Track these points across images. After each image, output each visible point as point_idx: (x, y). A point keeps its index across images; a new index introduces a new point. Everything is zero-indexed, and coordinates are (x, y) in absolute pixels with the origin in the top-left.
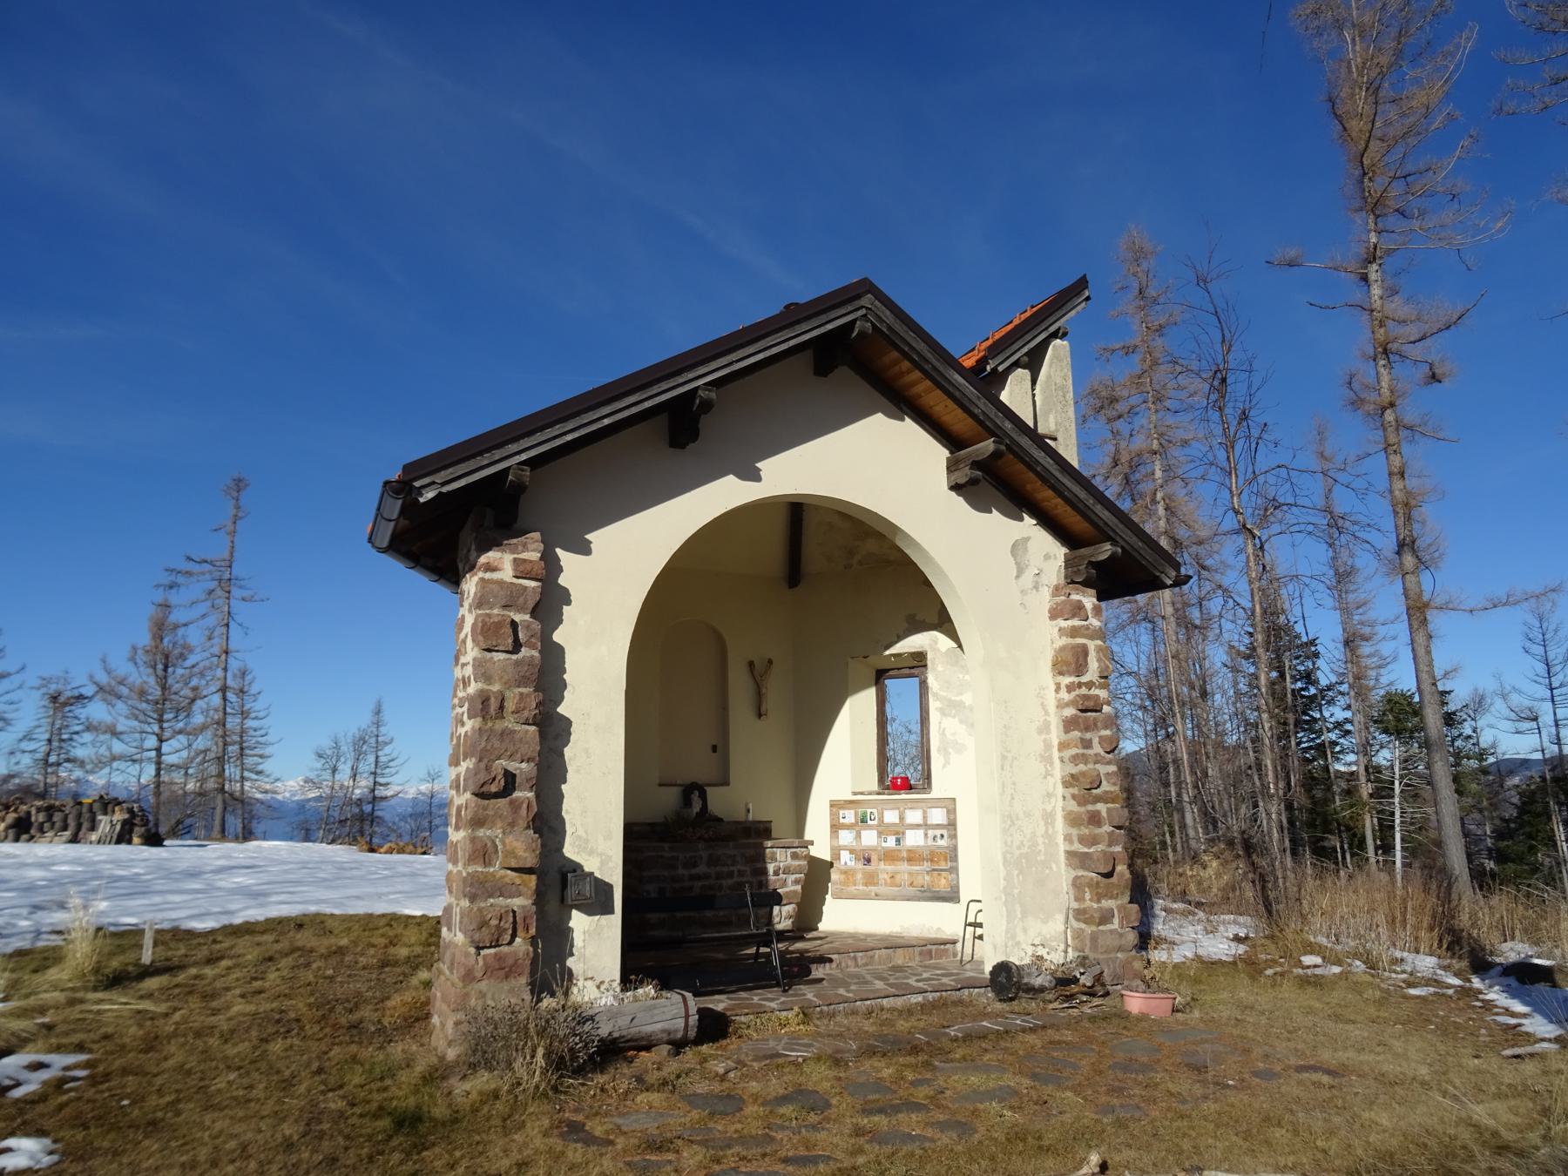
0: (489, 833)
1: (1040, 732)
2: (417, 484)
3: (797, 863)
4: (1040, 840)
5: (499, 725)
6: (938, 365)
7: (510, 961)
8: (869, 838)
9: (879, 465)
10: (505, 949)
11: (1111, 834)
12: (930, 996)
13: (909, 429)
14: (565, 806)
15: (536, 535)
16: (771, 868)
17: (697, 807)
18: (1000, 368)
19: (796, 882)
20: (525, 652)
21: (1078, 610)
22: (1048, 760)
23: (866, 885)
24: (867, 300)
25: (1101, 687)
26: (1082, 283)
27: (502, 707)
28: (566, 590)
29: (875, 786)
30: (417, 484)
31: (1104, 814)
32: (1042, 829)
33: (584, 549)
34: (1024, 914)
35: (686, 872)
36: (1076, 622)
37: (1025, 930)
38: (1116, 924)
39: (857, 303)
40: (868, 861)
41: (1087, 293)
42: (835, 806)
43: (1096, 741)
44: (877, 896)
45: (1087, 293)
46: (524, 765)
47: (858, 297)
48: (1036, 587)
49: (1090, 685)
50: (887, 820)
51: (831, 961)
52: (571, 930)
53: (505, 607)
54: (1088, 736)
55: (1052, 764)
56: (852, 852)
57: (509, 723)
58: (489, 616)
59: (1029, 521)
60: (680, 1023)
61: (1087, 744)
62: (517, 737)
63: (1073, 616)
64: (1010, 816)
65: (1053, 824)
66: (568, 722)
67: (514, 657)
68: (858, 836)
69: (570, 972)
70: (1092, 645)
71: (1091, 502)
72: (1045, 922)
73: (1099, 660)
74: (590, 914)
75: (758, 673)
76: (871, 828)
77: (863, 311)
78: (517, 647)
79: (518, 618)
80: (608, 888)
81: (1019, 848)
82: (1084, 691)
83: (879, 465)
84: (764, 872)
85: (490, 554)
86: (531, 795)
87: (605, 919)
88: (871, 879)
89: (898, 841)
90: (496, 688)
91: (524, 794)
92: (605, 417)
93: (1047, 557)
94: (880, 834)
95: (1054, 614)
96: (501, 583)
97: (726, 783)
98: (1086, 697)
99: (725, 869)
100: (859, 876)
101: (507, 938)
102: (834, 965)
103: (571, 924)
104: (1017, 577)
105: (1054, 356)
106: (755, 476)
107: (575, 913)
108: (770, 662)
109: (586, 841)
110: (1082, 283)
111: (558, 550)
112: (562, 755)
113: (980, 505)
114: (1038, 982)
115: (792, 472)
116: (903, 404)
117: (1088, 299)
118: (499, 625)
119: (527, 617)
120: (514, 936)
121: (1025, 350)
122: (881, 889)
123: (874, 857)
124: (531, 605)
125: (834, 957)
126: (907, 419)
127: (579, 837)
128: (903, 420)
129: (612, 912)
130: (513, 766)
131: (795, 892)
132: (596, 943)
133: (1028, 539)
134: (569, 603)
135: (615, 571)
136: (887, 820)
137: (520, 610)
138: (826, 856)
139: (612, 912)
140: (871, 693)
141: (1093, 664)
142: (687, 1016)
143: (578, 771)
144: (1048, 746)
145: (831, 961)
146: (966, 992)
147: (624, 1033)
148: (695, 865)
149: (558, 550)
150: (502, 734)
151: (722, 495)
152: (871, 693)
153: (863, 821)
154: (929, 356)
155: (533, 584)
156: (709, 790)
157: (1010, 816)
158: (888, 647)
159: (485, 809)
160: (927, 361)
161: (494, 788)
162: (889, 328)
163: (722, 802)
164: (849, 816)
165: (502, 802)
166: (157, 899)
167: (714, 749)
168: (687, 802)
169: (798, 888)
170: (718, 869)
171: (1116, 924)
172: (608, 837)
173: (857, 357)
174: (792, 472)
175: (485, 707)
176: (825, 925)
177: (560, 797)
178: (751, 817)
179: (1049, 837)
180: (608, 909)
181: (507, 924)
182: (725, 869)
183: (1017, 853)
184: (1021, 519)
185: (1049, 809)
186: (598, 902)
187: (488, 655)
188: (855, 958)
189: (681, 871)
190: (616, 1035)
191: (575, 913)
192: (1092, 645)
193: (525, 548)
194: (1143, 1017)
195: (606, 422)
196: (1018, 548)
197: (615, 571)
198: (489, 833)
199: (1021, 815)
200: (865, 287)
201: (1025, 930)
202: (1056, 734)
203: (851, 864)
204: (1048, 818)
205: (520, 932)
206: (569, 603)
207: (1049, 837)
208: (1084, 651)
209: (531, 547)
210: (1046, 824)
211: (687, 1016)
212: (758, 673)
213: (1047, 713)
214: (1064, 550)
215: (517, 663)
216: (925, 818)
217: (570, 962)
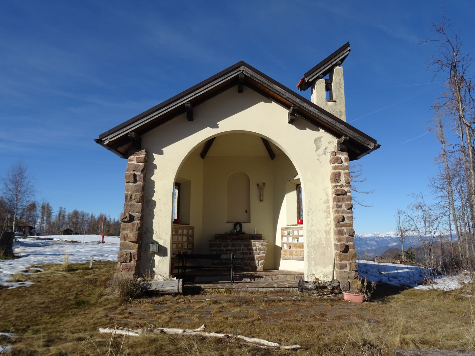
0: (126, 232)
1: (325, 203)
2: (103, 140)
3: (262, 247)
4: (323, 240)
5: (130, 203)
6: (269, 84)
7: (129, 267)
8: (291, 240)
9: (264, 119)
10: (128, 263)
11: (347, 238)
12: (277, 289)
13: (274, 105)
14: (153, 226)
15: (144, 150)
16: (254, 248)
17: (238, 229)
18: (310, 80)
19: (263, 253)
20: (138, 183)
21: (337, 160)
22: (328, 212)
23: (290, 255)
24: (242, 68)
25: (346, 186)
26: (347, 45)
27: (131, 198)
28: (156, 165)
29: (296, 223)
30: (103, 140)
31: (345, 231)
32: (325, 236)
33: (161, 153)
34: (316, 265)
35: (224, 249)
36: (337, 164)
37: (316, 270)
38: (348, 269)
39: (239, 69)
40: (290, 247)
41: (349, 48)
42: (283, 229)
43: (343, 205)
44: (292, 259)
45: (349, 48)
46: (137, 214)
47: (239, 67)
48: (325, 153)
49: (341, 186)
50: (295, 234)
51: (262, 277)
52: (154, 260)
53: (133, 171)
54: (340, 204)
55: (329, 213)
56: (286, 244)
57: (133, 202)
58: (128, 173)
59: (322, 131)
60: (176, 288)
61: (340, 207)
62: (135, 206)
63: (335, 162)
64: (311, 231)
65: (329, 234)
66: (155, 202)
67: (135, 184)
68: (288, 239)
69: (154, 272)
70: (342, 172)
71: (334, 122)
72: (325, 267)
73: (345, 177)
74: (160, 256)
75: (261, 187)
76: (291, 236)
77: (241, 71)
78: (135, 181)
79: (137, 173)
80: (166, 249)
81: (314, 242)
82: (338, 188)
83: (264, 119)
84: (252, 249)
85: (131, 157)
86: (138, 222)
87: (165, 258)
88: (291, 254)
89: (297, 241)
90: (130, 193)
91: (137, 222)
92: (156, 115)
93: (329, 143)
94: (293, 238)
95: (331, 162)
96: (133, 164)
97: (250, 222)
98: (338, 190)
99: (238, 248)
100: (288, 252)
101: (129, 260)
102: (263, 279)
103: (155, 259)
104: (316, 150)
105: (336, 73)
106: (217, 127)
107: (156, 255)
108: (264, 184)
109: (160, 235)
110: (347, 45)
111: (154, 154)
112: (153, 211)
113: (301, 127)
114: (309, 286)
115: (228, 124)
116: (270, 96)
117: (349, 50)
118: (130, 176)
119: (140, 173)
120: (131, 260)
121: (321, 72)
122: (293, 257)
123: (292, 246)
124: (141, 170)
125: (264, 276)
126: (273, 102)
127: (157, 234)
128: (271, 103)
129: (166, 255)
130: (133, 214)
131: (263, 256)
132: (162, 265)
133: (321, 137)
134: (156, 168)
135: (170, 160)
136: (295, 234)
137: (138, 171)
138: (280, 246)
139: (166, 255)
140: (294, 193)
141: (343, 179)
142: (178, 286)
143: (157, 216)
144: (328, 207)
145: (262, 277)
146: (291, 289)
147: (160, 289)
148: (227, 246)
149: (154, 154)
150: (131, 205)
151: (206, 133)
152: (294, 193)
153: (289, 234)
154: (266, 82)
155: (142, 164)
156: (243, 224)
157: (311, 231)
158: (295, 177)
159: (125, 225)
160: (265, 84)
161: (126, 220)
162: (251, 75)
163: (246, 228)
164: (286, 233)
165: (130, 224)
166: (56, 247)
167: (246, 211)
168: (235, 228)
169: (264, 255)
170: (235, 248)
171: (348, 269)
172: (166, 234)
173: (246, 87)
174: (228, 124)
175: (128, 198)
176: (281, 268)
177: (152, 223)
178: (256, 233)
179: (328, 239)
180: (165, 255)
181: (128, 256)
182: (238, 248)
183: (314, 244)
184: (319, 131)
185: (328, 229)
186: (162, 251)
187: (128, 184)
188: (271, 277)
189: (222, 248)
190: (157, 289)
191: (156, 255)
192: (342, 172)
193: (141, 154)
194: (347, 302)
195: (156, 117)
196: (317, 141)
197: (170, 160)
198: (126, 232)
199: (315, 231)
200: (242, 63)
201: (316, 270)
202: (331, 204)
203: (286, 248)
204: (327, 232)
205: (133, 259)
206: (156, 168)
207: (328, 239)
208: (339, 174)
209: (142, 154)
210: (326, 234)
211: (178, 286)
212: (261, 187)
213: (328, 196)
214: (337, 140)
215: (136, 186)
216: (298, 233)
217: (154, 269)
